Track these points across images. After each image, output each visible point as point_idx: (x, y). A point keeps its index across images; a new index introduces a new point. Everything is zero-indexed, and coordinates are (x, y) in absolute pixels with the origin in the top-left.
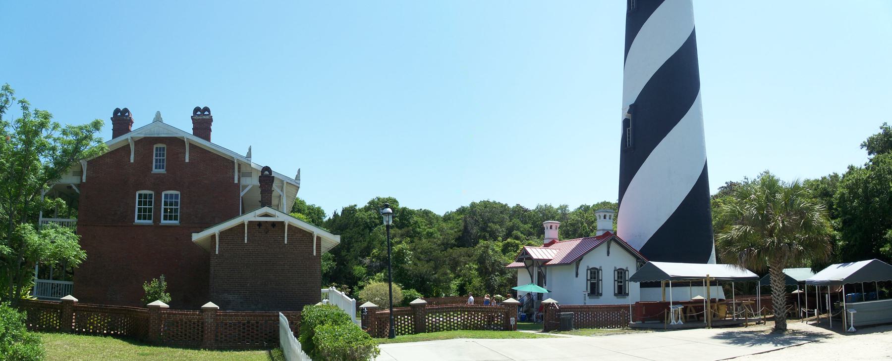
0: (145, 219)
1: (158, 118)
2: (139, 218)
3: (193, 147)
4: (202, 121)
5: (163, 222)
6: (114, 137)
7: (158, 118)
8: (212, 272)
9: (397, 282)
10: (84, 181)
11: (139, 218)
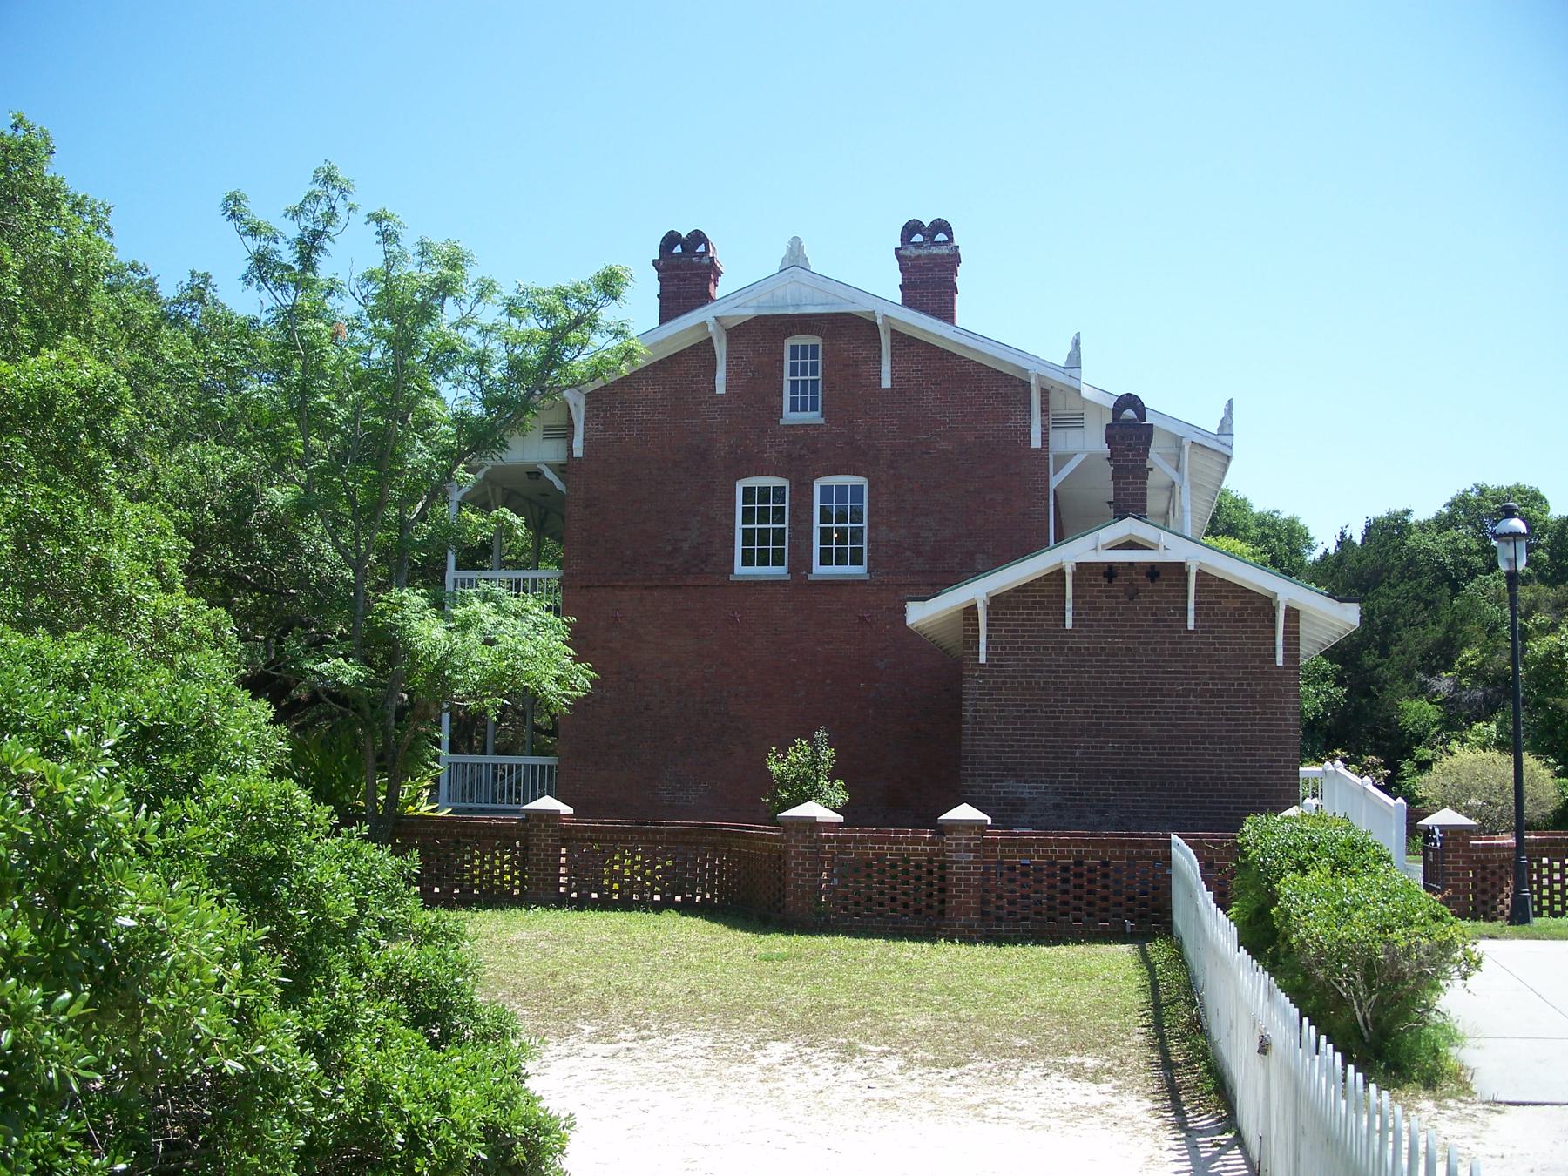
0: (840, 561)
1: (795, 259)
2: (747, 561)
3: (904, 342)
4: (929, 265)
5: (819, 570)
6: (665, 317)
7: (795, 259)
8: (968, 715)
9: (1539, 753)
10: (578, 453)
11: (747, 561)
